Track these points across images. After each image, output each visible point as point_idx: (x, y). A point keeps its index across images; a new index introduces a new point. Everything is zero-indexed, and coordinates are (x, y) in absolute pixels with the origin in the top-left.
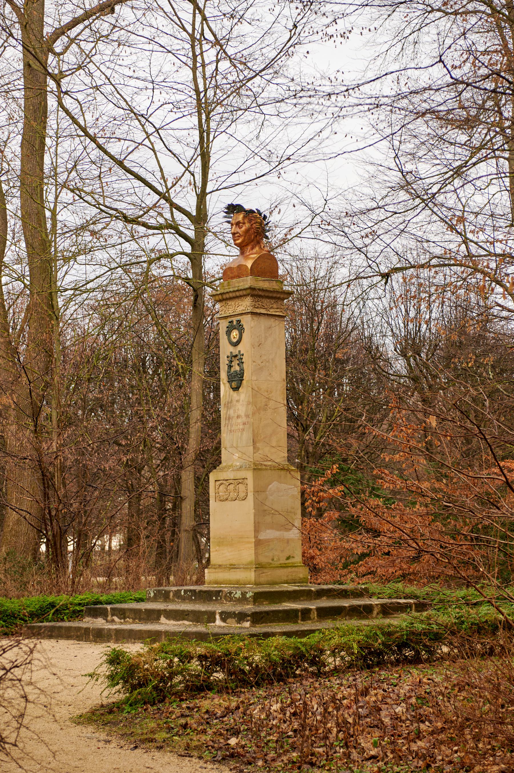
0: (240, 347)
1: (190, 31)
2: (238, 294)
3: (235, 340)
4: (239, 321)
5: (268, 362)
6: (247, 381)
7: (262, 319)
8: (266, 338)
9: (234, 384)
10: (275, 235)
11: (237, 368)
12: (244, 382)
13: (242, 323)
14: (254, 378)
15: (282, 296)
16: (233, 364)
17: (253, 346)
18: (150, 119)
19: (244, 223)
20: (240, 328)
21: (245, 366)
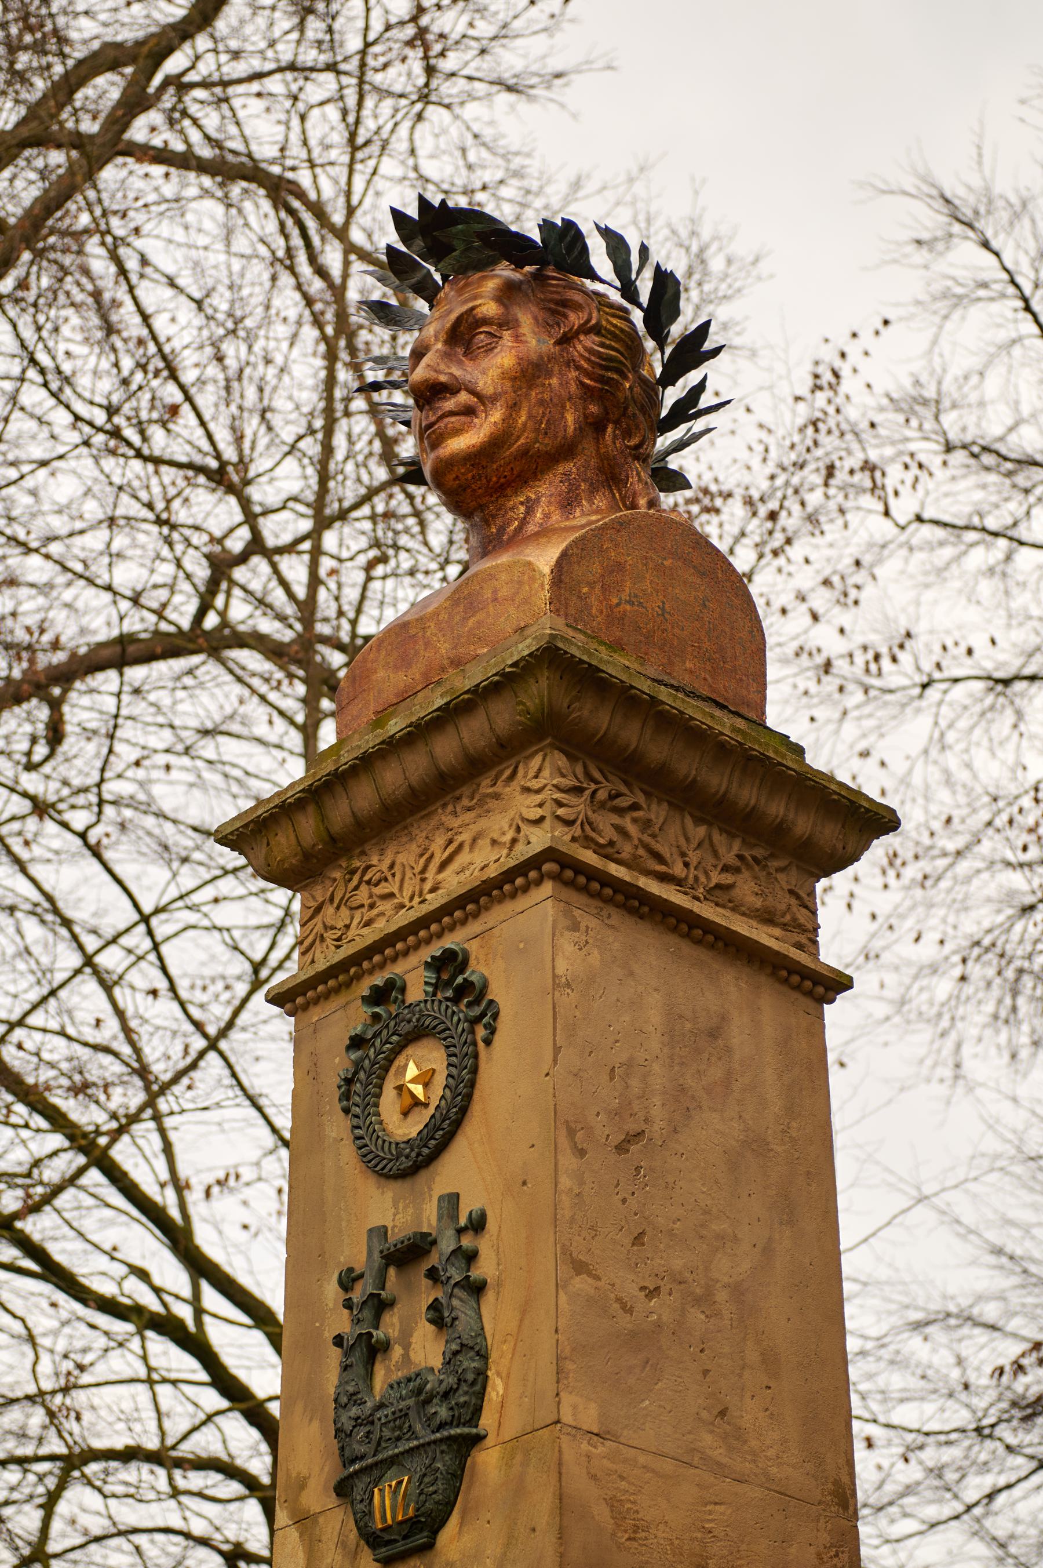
0: (465, 1172)
1: (301, 592)
2: (446, 748)
3: (404, 1129)
4: (450, 963)
5: (704, 1300)
6: (517, 1445)
7: (652, 953)
8: (683, 1104)
9: (389, 1501)
10: (721, 459)
11: (426, 1350)
12: (488, 1461)
13: (477, 969)
14: (581, 1409)
15: (803, 824)
16: (391, 1325)
17: (571, 1131)
18: (164, 949)
19: (506, 323)
20: (464, 1002)
21: (496, 1316)
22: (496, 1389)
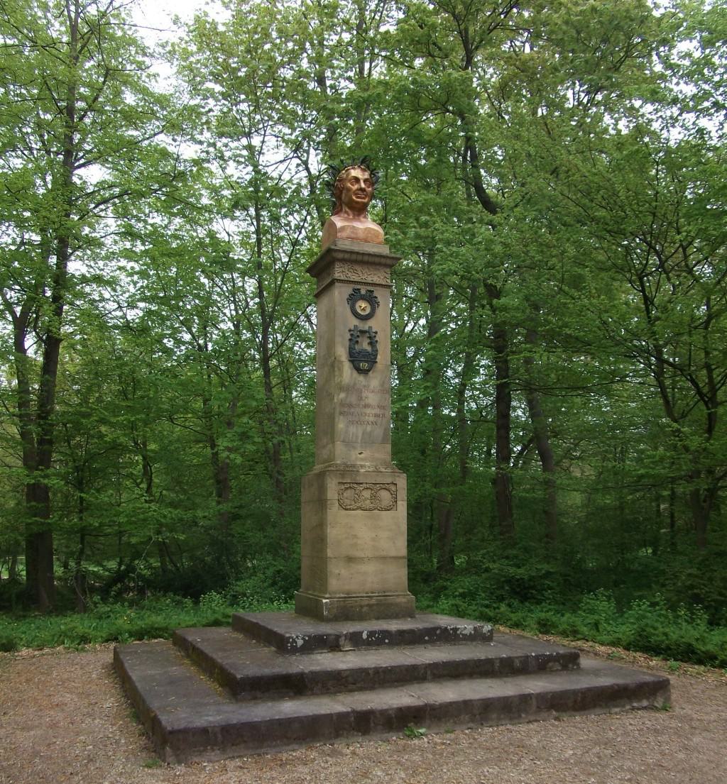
22: (379, 357)
